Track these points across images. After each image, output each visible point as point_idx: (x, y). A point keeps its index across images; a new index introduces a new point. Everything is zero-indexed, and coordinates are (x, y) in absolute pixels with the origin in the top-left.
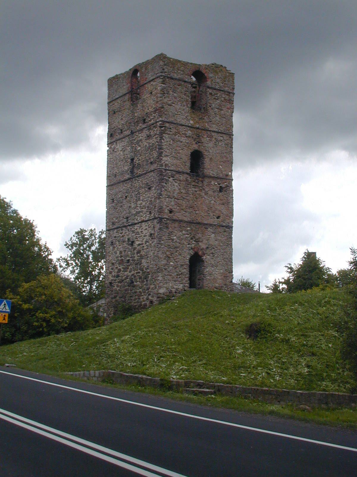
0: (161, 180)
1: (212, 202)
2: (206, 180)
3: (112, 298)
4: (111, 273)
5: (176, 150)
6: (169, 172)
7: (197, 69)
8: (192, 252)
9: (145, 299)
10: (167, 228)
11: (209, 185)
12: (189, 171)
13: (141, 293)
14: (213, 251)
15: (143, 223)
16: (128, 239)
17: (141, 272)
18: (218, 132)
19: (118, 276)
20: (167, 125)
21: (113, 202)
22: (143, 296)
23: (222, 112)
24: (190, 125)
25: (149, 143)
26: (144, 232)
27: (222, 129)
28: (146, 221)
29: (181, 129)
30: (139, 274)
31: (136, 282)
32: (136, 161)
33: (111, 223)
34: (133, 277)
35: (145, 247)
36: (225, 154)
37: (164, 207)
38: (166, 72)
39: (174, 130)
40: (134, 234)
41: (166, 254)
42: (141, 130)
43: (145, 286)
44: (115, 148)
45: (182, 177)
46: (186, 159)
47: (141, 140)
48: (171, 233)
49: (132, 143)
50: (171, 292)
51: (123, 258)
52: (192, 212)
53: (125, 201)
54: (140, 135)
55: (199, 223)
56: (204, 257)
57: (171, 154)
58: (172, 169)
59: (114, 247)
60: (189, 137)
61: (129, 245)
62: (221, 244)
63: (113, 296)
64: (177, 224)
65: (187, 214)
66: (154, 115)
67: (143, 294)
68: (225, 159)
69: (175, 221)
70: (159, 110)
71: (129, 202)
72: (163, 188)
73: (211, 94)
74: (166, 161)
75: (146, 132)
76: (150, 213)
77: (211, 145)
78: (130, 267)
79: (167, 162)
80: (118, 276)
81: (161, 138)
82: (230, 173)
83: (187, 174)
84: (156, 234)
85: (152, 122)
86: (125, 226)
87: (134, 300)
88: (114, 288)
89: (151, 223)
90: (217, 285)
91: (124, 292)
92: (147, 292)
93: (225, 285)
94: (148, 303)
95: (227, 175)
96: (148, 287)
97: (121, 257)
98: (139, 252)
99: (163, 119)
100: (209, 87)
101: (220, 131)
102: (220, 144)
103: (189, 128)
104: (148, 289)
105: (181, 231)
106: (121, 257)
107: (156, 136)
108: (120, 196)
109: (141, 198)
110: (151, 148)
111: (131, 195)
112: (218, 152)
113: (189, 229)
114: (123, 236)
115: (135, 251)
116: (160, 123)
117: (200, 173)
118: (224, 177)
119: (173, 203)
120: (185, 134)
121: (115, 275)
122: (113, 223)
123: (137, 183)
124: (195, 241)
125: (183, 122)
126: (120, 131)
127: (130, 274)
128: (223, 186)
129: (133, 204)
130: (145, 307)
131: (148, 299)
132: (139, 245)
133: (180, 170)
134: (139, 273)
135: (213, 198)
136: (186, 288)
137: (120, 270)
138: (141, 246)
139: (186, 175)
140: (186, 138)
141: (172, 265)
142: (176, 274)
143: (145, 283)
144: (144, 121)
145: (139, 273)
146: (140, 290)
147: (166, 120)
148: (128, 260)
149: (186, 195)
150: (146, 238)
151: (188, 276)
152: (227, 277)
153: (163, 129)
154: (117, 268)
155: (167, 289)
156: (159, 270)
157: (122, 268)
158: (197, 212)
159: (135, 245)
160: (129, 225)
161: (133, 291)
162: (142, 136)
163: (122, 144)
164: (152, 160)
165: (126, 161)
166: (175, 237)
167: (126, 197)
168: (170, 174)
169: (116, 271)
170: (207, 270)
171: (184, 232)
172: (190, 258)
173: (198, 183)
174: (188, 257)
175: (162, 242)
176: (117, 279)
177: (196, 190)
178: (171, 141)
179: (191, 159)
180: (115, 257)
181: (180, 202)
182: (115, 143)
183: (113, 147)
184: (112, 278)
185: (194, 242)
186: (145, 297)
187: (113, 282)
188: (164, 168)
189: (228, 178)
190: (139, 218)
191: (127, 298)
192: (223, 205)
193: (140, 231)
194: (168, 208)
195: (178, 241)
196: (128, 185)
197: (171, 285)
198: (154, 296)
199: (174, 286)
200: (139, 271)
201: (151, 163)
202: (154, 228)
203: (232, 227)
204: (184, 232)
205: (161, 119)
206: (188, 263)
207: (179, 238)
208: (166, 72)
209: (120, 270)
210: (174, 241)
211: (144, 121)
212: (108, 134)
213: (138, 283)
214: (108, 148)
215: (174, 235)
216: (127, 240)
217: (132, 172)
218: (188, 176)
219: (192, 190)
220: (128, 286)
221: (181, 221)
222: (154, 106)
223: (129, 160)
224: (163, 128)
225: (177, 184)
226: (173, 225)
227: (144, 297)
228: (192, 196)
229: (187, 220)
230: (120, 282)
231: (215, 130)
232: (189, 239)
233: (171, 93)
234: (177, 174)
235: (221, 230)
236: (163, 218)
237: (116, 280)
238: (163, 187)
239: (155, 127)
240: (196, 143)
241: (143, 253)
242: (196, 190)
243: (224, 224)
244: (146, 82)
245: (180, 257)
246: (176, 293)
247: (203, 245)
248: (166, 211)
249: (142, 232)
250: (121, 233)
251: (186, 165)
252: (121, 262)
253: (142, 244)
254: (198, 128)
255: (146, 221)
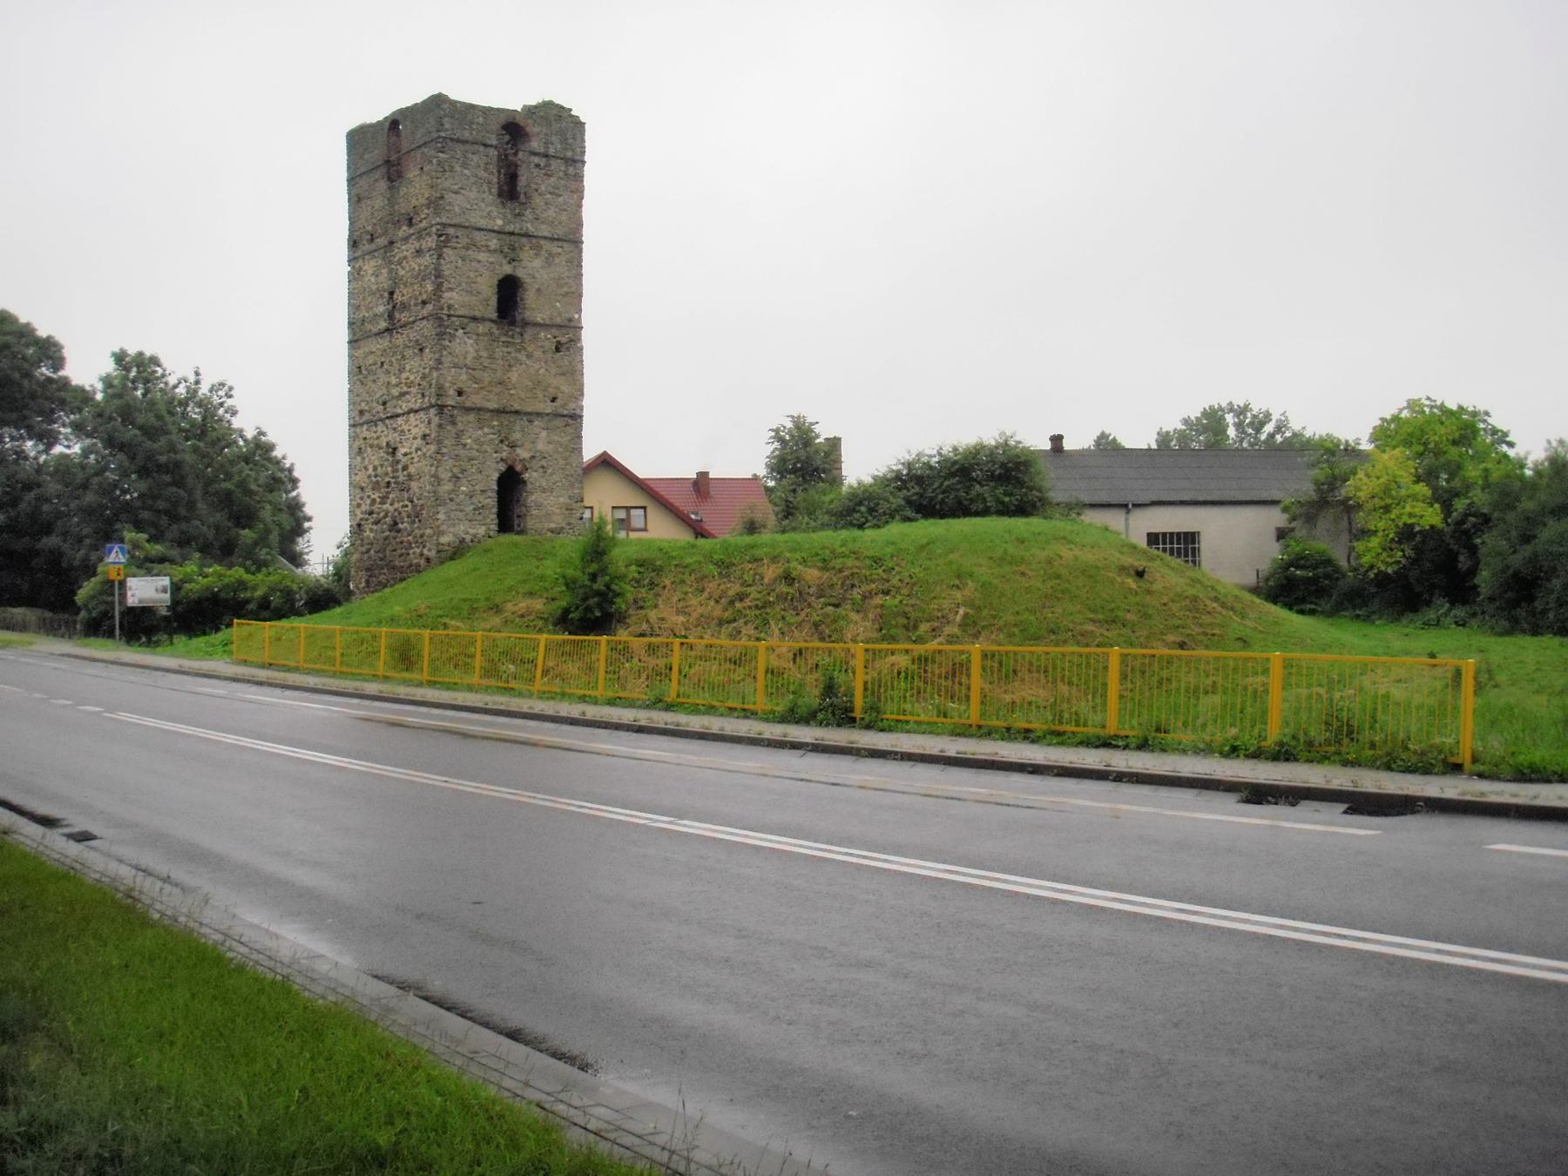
0: (440, 335)
1: (542, 371)
2: (529, 332)
3: (363, 553)
4: (359, 506)
5: (468, 277)
6: (454, 319)
7: (511, 120)
8: (503, 467)
10: (454, 423)
11: (535, 338)
12: (494, 315)
14: (544, 463)
15: (412, 415)
16: (388, 444)
17: (409, 504)
18: (552, 239)
19: (371, 513)
20: (451, 231)
21: (360, 371)
23: (561, 199)
24: (496, 228)
25: (420, 265)
26: (414, 431)
27: (559, 232)
28: (416, 411)
29: (478, 236)
32: (398, 297)
33: (357, 413)
34: (396, 514)
35: (416, 460)
36: (567, 280)
37: (447, 385)
38: (447, 130)
39: (464, 241)
40: (396, 435)
41: (451, 471)
42: (406, 239)
43: (416, 531)
44: (360, 269)
45: (481, 328)
46: (490, 294)
47: (405, 258)
48: (459, 435)
49: (391, 262)
50: (462, 541)
51: (379, 479)
53: (379, 371)
54: (404, 247)
55: (517, 412)
56: (527, 475)
57: (460, 285)
58: (460, 313)
59: (363, 459)
60: (495, 251)
61: (388, 453)
62: (560, 450)
63: (364, 549)
64: (472, 417)
66: (426, 211)
68: (565, 289)
69: (468, 410)
70: (436, 204)
71: (388, 372)
73: (538, 166)
74: (451, 298)
75: (413, 245)
76: (423, 395)
77: (537, 263)
78: (391, 496)
79: (451, 302)
80: (371, 513)
81: (440, 256)
82: (576, 316)
83: (492, 321)
84: (433, 436)
85: (424, 224)
86: (382, 420)
90: (553, 526)
93: (569, 524)
94: (422, 562)
95: (570, 320)
97: (376, 476)
98: (405, 468)
99: (444, 220)
100: (535, 154)
101: (555, 236)
102: (557, 261)
103: (494, 235)
105: (481, 428)
106: (376, 476)
107: (432, 252)
108: (371, 362)
109: (408, 367)
110: (421, 277)
111: (391, 362)
112: (552, 276)
113: (495, 423)
114: (378, 438)
115: (400, 467)
116: (438, 227)
117: (518, 318)
118: (566, 323)
119: (464, 377)
120: (488, 246)
122: (361, 412)
123: (400, 340)
124: (508, 446)
125: (482, 223)
126: (369, 237)
127: (391, 509)
128: (563, 340)
129: (393, 377)
130: (418, 570)
131: (422, 555)
132: (405, 454)
133: (478, 314)
134: (407, 506)
135: (543, 364)
136: (491, 533)
137: (374, 501)
138: (409, 456)
139: (488, 324)
140: (488, 254)
141: (463, 491)
142: (472, 507)
143: (416, 525)
144: (410, 222)
145: (407, 506)
147: (449, 222)
148: (389, 483)
149: (489, 361)
150: (416, 441)
151: (495, 510)
152: (572, 510)
153: (442, 238)
154: (369, 497)
155: (455, 535)
156: (438, 500)
158: (512, 392)
159: (399, 455)
160: (388, 418)
162: (406, 250)
163: (373, 263)
164: (424, 297)
165: (381, 296)
166: (469, 441)
167: (382, 363)
168: (457, 323)
169: (368, 502)
170: (533, 498)
171: (486, 430)
172: (499, 478)
173: (513, 337)
174: (496, 476)
175: (444, 450)
177: (509, 350)
178: (460, 261)
179: (498, 293)
181: (477, 374)
182: (361, 260)
183: (357, 266)
185: (506, 448)
188: (445, 312)
189: (572, 324)
190: (404, 405)
191: (388, 553)
192: (563, 377)
193: (406, 428)
194: (455, 387)
195: (475, 447)
196: (384, 342)
197: (462, 527)
199: (470, 530)
200: (407, 502)
201: (424, 303)
202: (429, 423)
203: (581, 417)
204: (486, 430)
205: (438, 220)
206: (495, 487)
207: (476, 441)
208: (447, 130)
209: (374, 501)
210: (468, 447)
211: (410, 222)
212: (349, 240)
213: (405, 525)
214: (349, 269)
216: (385, 444)
217: (391, 316)
218: (493, 325)
219: (500, 351)
220: (390, 531)
221: (480, 409)
222: (427, 195)
223: (386, 295)
224: (444, 240)
225: (472, 341)
226: (466, 418)
228: (500, 361)
229: (491, 408)
230: (376, 523)
231: (546, 234)
233: (458, 168)
235: (559, 422)
236: (447, 406)
238: (445, 348)
239: (429, 234)
240: (510, 263)
241: (412, 470)
242: (509, 350)
243: (565, 412)
244: (413, 146)
245: (479, 476)
246: (472, 541)
247: (523, 454)
248: (451, 392)
249: (409, 430)
250: (375, 432)
251: (488, 305)
252: (376, 486)
253: (411, 453)
254: (512, 234)
255: (416, 411)
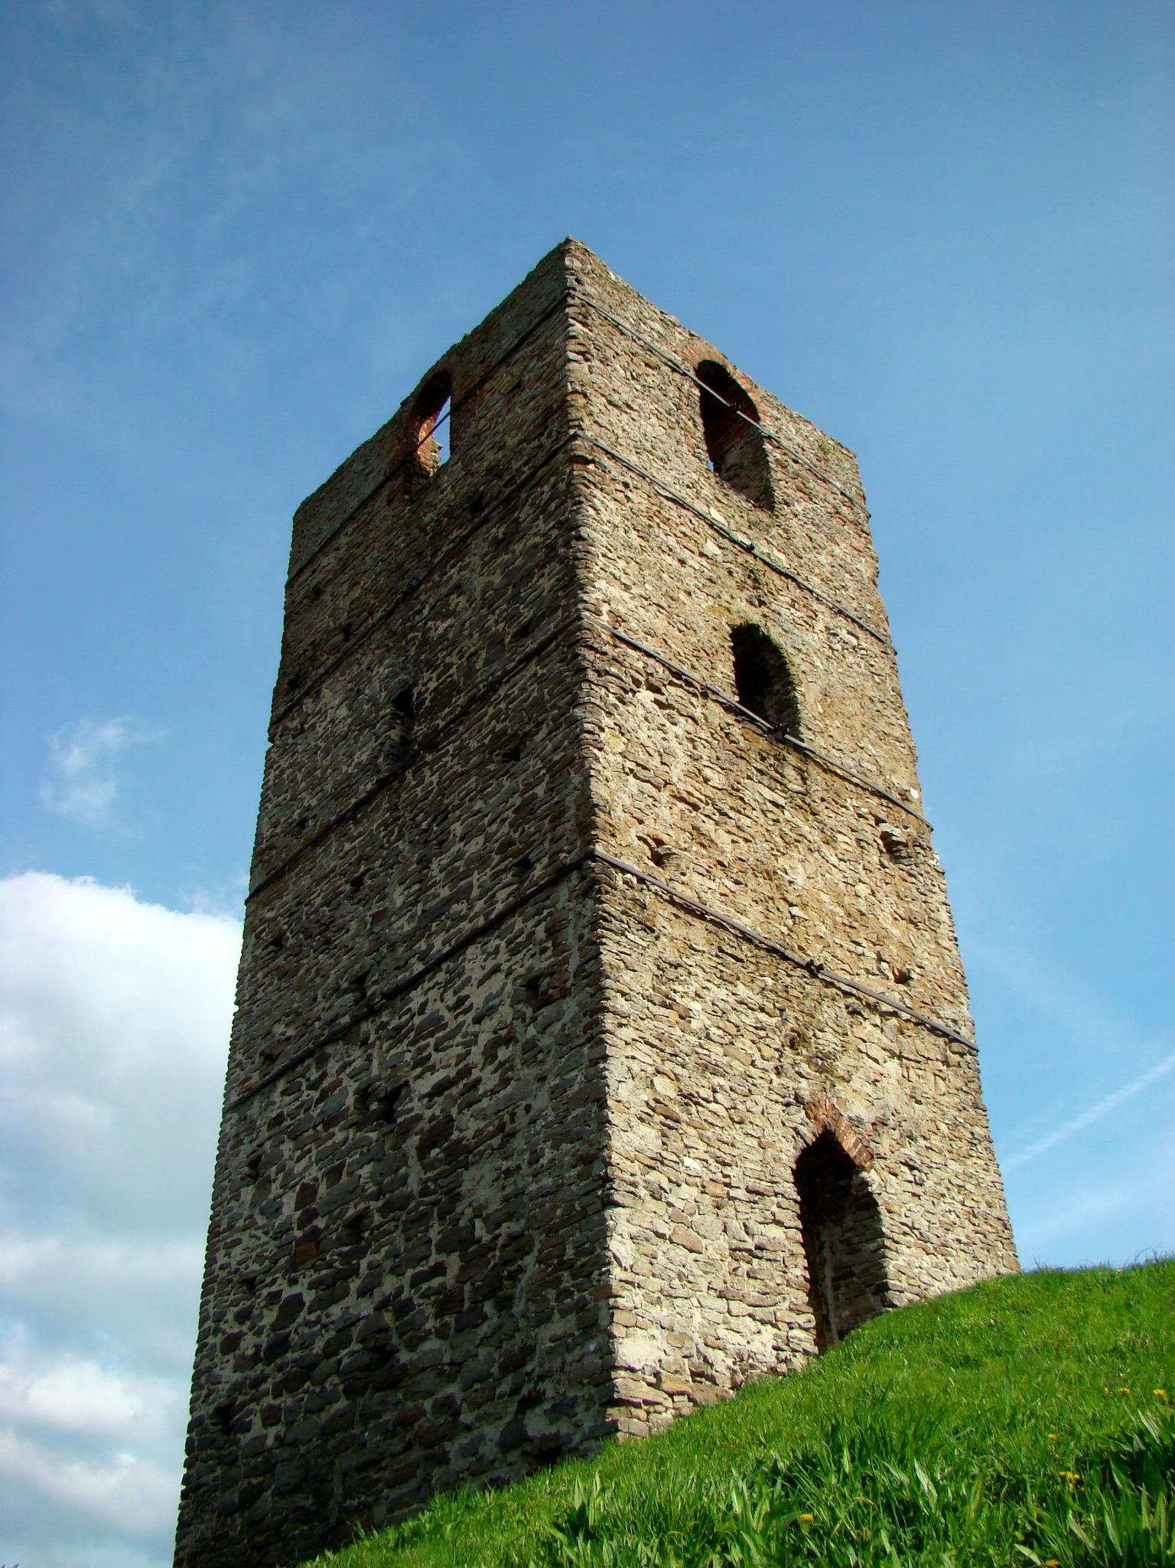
3: (227, 1512)
9: (488, 1450)
13: (457, 1414)
22: (468, 1428)
30: (436, 1282)
31: (412, 1347)
34: (388, 1317)
52: (772, 898)
65: (745, 900)
67: (466, 1418)
72: (609, 714)
87: (392, 1484)
88: (245, 1439)
89: (478, 1081)
91: (315, 1442)
92: (505, 1387)
96: (511, 1346)
104: (514, 1364)
121: (258, 1347)
134: (439, 1269)
146: (453, 1389)
151: (799, 1271)
157: (311, 1287)
158: (795, 911)
161: (388, 1417)
172: (799, 1161)
174: (789, 1152)
176: (268, 1370)
180: (265, 1239)
184: (237, 1377)
186: (492, 1432)
187: (240, 1399)
198: (573, 1402)
215: (691, 990)
227: (482, 1437)
232: (777, 1042)
234: (671, 683)
237: (263, 1378)
